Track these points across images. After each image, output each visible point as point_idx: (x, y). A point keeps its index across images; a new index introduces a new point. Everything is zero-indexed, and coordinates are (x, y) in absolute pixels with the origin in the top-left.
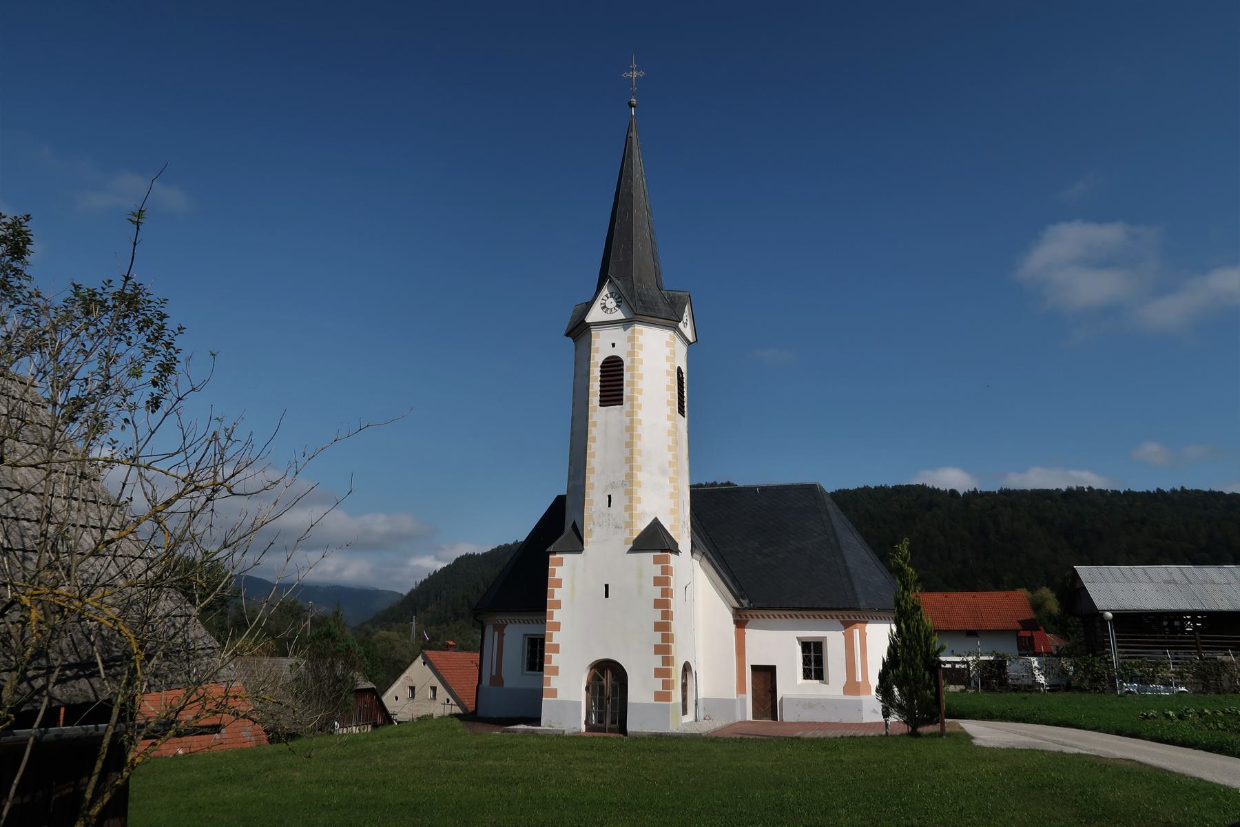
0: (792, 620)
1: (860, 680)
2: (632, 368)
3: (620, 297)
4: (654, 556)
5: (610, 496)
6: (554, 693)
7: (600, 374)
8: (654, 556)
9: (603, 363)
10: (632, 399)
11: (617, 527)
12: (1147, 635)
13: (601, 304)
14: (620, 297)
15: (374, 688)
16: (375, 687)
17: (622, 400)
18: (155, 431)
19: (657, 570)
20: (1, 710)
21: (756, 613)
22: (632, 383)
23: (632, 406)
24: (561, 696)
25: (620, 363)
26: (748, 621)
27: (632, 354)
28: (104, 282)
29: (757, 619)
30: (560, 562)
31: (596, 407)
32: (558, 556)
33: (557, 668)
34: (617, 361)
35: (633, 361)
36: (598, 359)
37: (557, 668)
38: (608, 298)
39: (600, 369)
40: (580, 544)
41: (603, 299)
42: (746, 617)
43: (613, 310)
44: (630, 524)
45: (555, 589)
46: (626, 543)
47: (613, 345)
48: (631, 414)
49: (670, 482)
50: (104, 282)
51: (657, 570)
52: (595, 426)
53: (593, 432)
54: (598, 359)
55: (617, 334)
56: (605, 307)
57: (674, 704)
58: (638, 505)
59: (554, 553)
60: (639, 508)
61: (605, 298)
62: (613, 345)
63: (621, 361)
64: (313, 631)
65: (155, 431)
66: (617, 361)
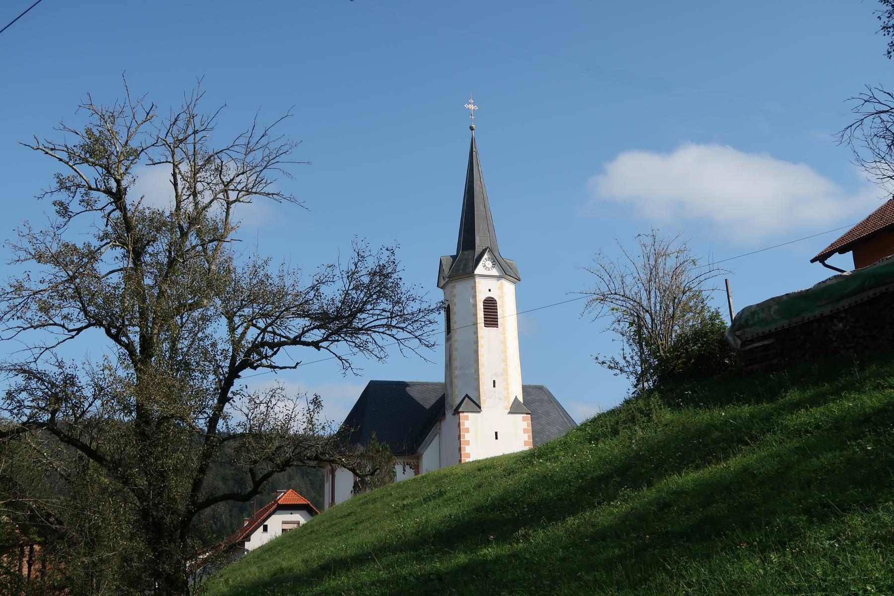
3: (494, 261)
4: (523, 417)
6: (454, 287)
7: (483, 307)
8: (523, 417)
9: (485, 300)
11: (500, 399)
12: (687, 478)
14: (494, 261)
18: (149, 112)
23: (504, 329)
25: (494, 302)
27: (501, 297)
28: (713, 285)
30: (467, 418)
31: (482, 327)
32: (465, 414)
34: (494, 303)
35: (503, 302)
36: (481, 297)
39: (482, 304)
44: (508, 398)
45: (465, 421)
46: (506, 409)
47: (490, 290)
48: (504, 333)
50: (713, 285)
52: (483, 338)
53: (481, 342)
54: (481, 297)
55: (493, 284)
56: (485, 266)
59: (463, 412)
61: (484, 262)
62: (490, 290)
63: (496, 301)
65: (149, 112)
66: (493, 301)
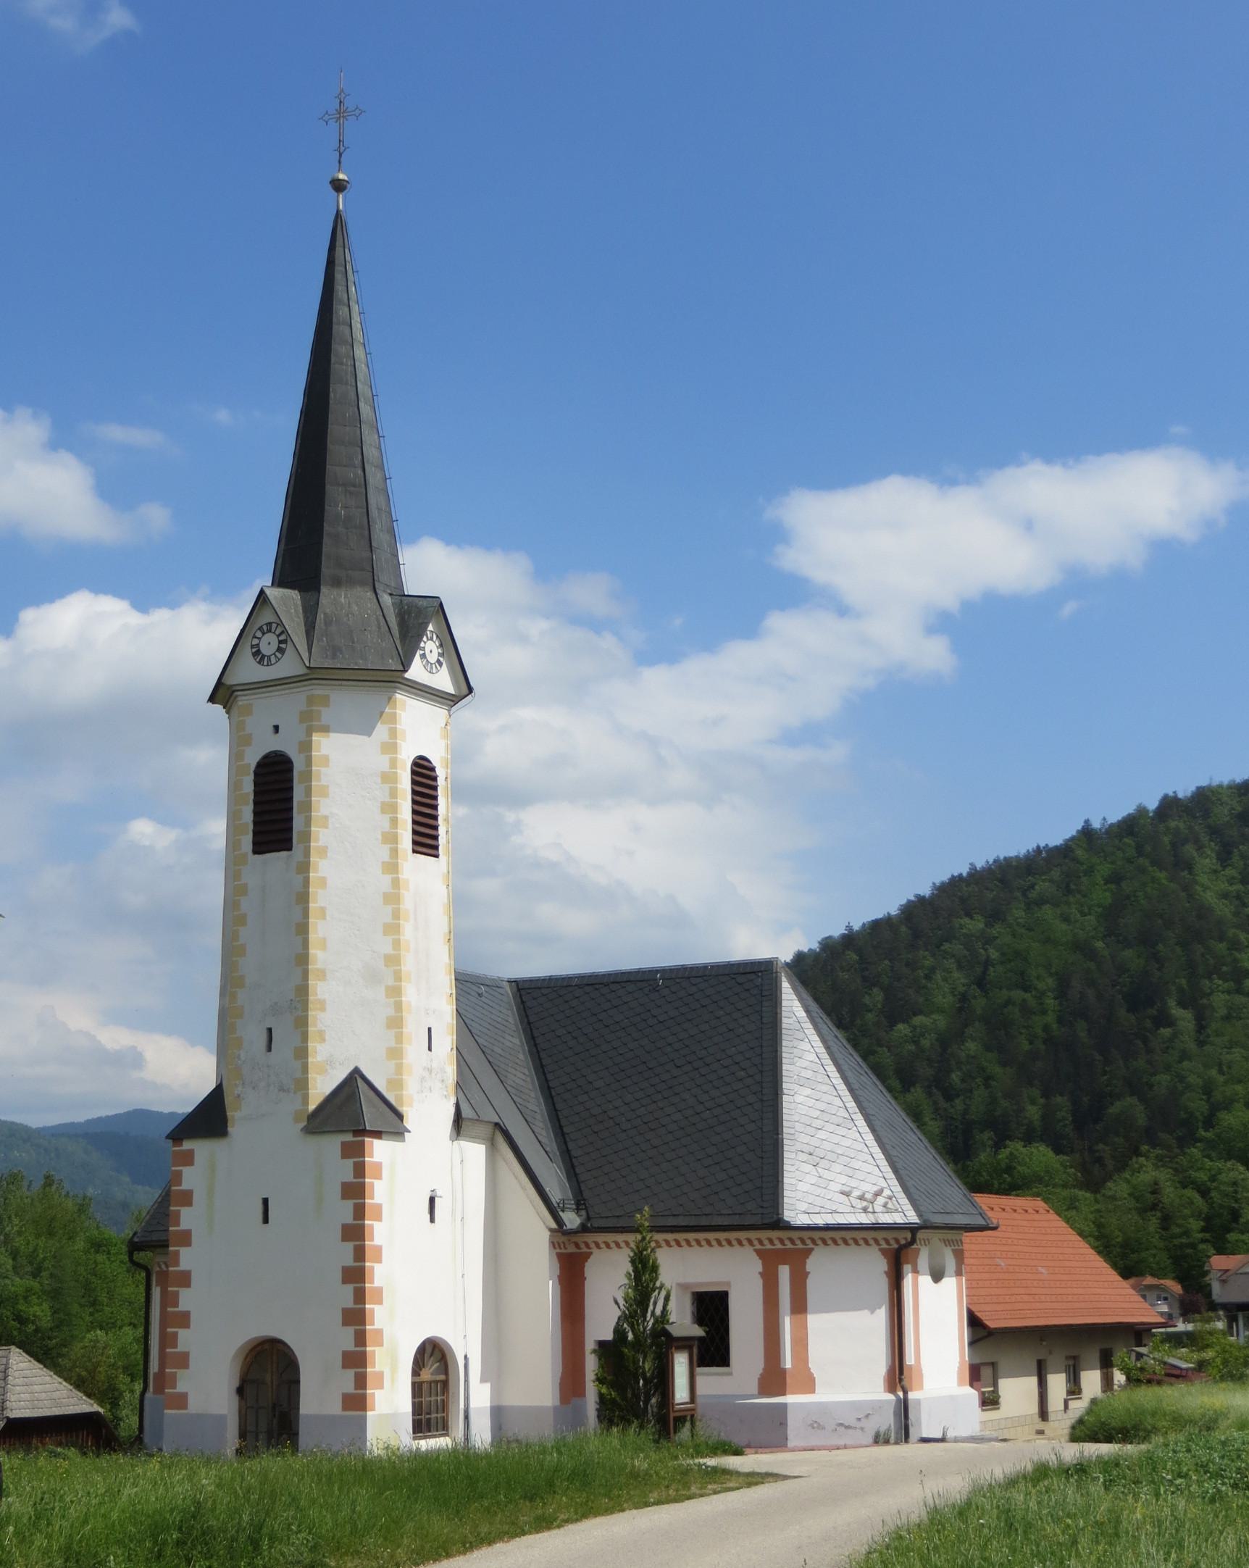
0: (742, 1249)
1: (913, 1363)
2: (308, 776)
5: (270, 1030)
6: (181, 1401)
10: (307, 837)
13: (252, 647)
15: (97, 1413)
16: (101, 1410)
17: (291, 839)
19: (345, 1171)
20: (103, 1562)
21: (605, 1239)
22: (307, 807)
23: (307, 853)
24: (195, 1405)
26: (591, 1253)
29: (688, 1248)
33: (345, 1366)
37: (345, 1366)
38: (264, 634)
40: (460, 1102)
41: (255, 637)
42: (587, 1245)
43: (273, 657)
44: (302, 1085)
46: (297, 1120)
48: (304, 868)
49: (387, 996)
51: (345, 1171)
56: (258, 652)
57: (380, 1415)
58: (319, 1047)
60: (319, 1052)
61: (259, 634)
64: (8, 1308)
